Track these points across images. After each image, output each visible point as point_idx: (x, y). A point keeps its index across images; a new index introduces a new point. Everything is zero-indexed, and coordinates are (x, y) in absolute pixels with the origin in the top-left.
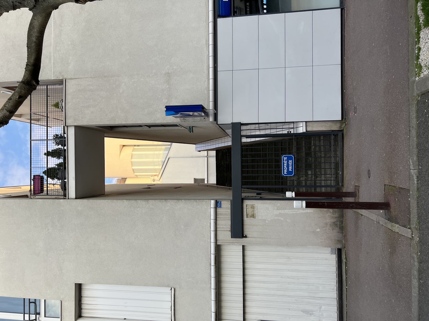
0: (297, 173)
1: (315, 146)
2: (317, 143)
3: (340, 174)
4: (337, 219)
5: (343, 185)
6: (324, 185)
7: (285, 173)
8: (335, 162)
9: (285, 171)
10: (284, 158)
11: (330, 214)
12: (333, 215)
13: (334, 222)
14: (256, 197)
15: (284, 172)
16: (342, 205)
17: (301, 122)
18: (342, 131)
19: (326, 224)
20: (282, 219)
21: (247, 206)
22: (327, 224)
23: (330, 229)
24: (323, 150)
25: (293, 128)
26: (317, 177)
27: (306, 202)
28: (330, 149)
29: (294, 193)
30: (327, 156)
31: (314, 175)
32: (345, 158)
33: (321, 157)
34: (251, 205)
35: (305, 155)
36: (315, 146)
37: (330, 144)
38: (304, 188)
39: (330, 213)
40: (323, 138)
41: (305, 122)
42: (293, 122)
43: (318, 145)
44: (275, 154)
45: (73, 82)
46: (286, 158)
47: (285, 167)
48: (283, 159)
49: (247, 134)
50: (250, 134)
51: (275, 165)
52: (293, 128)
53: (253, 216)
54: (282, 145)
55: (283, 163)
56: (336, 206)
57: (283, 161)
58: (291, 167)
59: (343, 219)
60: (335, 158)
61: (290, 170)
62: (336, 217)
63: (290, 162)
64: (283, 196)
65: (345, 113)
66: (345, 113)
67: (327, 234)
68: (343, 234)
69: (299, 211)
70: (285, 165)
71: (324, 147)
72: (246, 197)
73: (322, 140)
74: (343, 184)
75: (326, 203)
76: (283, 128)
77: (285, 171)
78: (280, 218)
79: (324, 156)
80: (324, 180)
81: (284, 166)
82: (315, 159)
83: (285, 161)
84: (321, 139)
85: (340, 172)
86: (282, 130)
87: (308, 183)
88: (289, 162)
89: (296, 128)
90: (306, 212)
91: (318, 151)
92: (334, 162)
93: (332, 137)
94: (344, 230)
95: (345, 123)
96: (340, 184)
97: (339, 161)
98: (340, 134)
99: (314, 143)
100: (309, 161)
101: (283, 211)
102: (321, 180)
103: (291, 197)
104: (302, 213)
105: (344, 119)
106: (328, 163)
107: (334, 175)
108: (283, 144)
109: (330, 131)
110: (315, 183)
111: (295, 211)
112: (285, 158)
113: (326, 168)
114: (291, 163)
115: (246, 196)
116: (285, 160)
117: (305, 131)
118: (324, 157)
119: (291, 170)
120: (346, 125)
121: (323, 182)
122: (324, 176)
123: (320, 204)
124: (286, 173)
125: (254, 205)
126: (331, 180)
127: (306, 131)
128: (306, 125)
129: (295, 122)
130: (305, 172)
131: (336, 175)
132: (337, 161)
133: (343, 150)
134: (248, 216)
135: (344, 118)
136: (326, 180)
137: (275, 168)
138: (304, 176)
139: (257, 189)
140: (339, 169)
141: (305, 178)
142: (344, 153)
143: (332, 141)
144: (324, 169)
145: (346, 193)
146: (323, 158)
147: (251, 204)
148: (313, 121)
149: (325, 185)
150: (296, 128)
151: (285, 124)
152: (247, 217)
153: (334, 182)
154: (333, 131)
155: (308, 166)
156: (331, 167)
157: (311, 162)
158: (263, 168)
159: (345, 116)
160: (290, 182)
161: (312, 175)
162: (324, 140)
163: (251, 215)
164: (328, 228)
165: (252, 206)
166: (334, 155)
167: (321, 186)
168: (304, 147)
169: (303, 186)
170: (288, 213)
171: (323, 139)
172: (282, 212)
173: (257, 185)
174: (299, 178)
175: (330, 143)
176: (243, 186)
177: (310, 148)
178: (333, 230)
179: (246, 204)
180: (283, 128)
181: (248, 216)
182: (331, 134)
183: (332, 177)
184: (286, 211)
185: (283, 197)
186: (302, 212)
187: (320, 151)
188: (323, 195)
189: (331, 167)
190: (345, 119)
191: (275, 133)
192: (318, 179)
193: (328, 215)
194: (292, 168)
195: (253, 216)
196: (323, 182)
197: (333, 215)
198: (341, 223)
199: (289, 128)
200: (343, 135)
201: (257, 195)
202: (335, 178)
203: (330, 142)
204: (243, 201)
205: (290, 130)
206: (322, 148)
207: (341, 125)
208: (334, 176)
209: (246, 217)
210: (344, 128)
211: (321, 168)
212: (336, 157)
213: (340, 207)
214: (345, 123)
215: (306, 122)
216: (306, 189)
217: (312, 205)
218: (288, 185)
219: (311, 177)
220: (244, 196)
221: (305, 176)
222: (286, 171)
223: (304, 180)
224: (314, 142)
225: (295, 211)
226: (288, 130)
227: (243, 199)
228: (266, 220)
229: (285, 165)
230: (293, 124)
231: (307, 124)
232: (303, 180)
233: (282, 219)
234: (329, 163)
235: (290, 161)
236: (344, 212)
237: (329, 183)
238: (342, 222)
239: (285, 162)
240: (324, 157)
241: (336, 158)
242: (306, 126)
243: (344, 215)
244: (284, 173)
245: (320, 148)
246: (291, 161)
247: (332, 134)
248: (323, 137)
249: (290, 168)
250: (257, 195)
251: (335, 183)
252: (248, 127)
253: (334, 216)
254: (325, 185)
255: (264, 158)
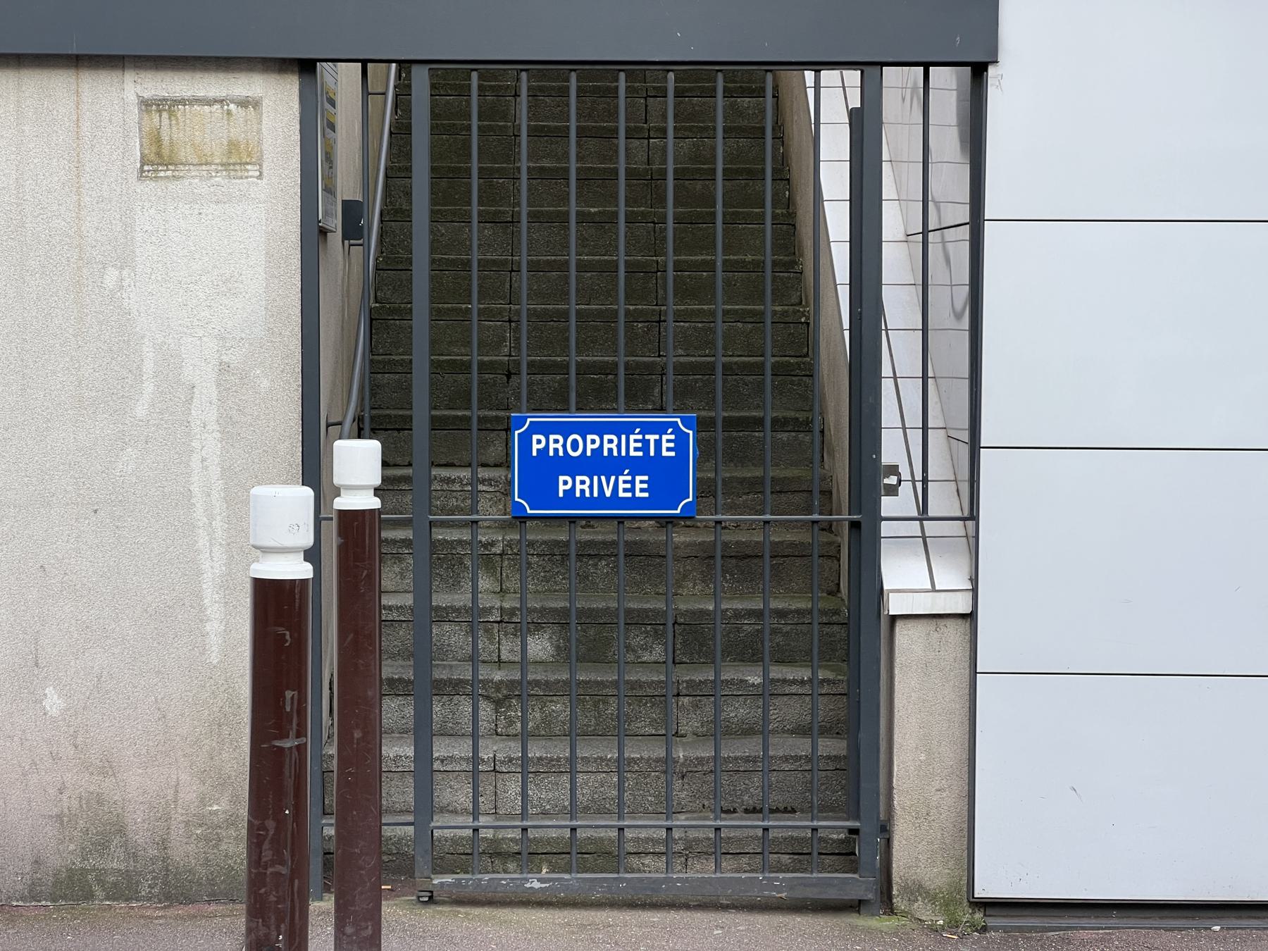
0: (531, 544)
1: (768, 692)
2: (788, 711)
3: (527, 880)
4: (153, 852)
5: (432, 900)
6: (436, 755)
7: (535, 437)
8: (630, 847)
9: (556, 444)
10: (665, 437)
11: (189, 794)
12: (187, 823)
13: (121, 831)
14: (330, 190)
15: (547, 429)
16: (284, 870)
17: (974, 580)
18: (886, 902)
19: (107, 768)
20: (141, 410)
21: (244, 103)
22: (103, 772)
23: (64, 797)
24: (724, 754)
25: (923, 515)
26: (498, 703)
27: (304, 582)
28: (735, 811)
29: (371, 502)
30: (678, 784)
31: (517, 676)
32: (655, 917)
33: (672, 736)
34: (260, 142)
35: (683, 614)
36: (768, 692)
37: (777, 811)
38: (408, 600)
39: (203, 801)
40: (829, 757)
41: (963, 606)
42: (973, 515)
43: (773, 714)
44: (709, 369)
45: (344, 196)
46: (665, 453)
47: (592, 443)
48: (660, 429)
49: (886, 168)
50: (885, 156)
51: (611, 369)
52: (923, 515)
53: (159, 154)
54: (779, 424)
55: (628, 429)
56: (271, 824)
57: (647, 428)
58: (586, 487)
59: (149, 899)
60: (655, 842)
61: (564, 483)
62: (164, 844)
63: (633, 482)
64: (340, 424)
65: (1031, 929)
66: (1031, 929)
67: (24, 775)
68: (22, 898)
69: (215, 549)
70: (610, 444)
71: (747, 760)
72: (327, 106)
73: (814, 747)
74: (443, 903)
75: (298, 747)
76: (925, 428)
77: (560, 438)
78: (149, 387)
79: (675, 761)
80: (475, 759)
81: (601, 429)
82: (650, 692)
83: (646, 443)
84: (821, 742)
85: (539, 880)
86: (914, 419)
87: (453, 637)
88: (633, 474)
89: (924, 538)
90: (202, 609)
91: (724, 715)
92: (629, 834)
93: (834, 827)
94: (58, 909)
95: (953, 925)
96: (448, 879)
97: (633, 871)
98: (858, 885)
99: (785, 681)
100: (634, 643)
101: (212, 415)
102: (475, 736)
103: (336, 481)
104: (199, 573)
105: (978, 915)
106: (615, 793)
107: (517, 834)
108: (784, 436)
109: (882, 808)
110: (453, 688)
111: (211, 518)
112: (665, 445)
113: (580, 778)
114: (621, 494)
115: (332, 103)
116: (652, 438)
117: (895, 606)
118: (668, 760)
119: (562, 488)
120: (934, 930)
121: (462, 749)
122: (511, 760)
123: (289, 694)
124: (535, 447)
125: (253, 171)
126: (475, 814)
127: (894, 619)
128: (942, 622)
129: (971, 532)
130: (542, 612)
131: (516, 848)
132: (634, 861)
133: (725, 908)
134: (160, 111)
135: (991, 922)
136: (475, 773)
137: (583, 369)
138: (507, 605)
139: (397, 213)
140: (567, 876)
141: (489, 611)
142: (699, 916)
143: (799, 825)
144: (572, 759)
145: (375, 917)
146: (663, 754)
147: (267, 146)
148: (974, 672)
149: (437, 766)
150: (924, 538)
151: (964, 451)
152: (146, 105)
153: (459, 832)
154: (885, 830)
155: (592, 632)
156: (586, 809)
157: (631, 657)
158: (579, 263)
159: (1006, 930)
160: (457, 487)
161: (524, 663)
162: (809, 759)
163: (166, 139)
164: (68, 777)
165: (249, 155)
166: (686, 840)
167: (423, 733)
168: (757, 604)
169: (423, 592)
170: (196, 458)
171: (822, 751)
172: (205, 411)
173: (435, 217)
174: (488, 561)
175: (785, 811)
176: (421, 79)
177: (748, 652)
178: (59, 817)
179: (265, 102)
180: (925, 428)
181: (160, 111)
182: (857, 818)
183: (498, 820)
184: (209, 446)
185: (328, 426)
186: (208, 576)
187: (718, 731)
188: (357, 734)
189: (586, 809)
190: (984, 929)
191: (886, 370)
192: (486, 710)
193: (184, 777)
194: (584, 502)
195: (159, 154)
196: (462, 749)
197: (187, 823)
198: (115, 885)
199: (925, 481)
200: (855, 907)
201: (346, 204)
202: (494, 841)
203: (793, 811)
204: (293, 72)
205: (905, 488)
206: (749, 747)
207: (931, 897)
208: (510, 834)
209: (147, 95)
210: (904, 914)
211: (573, 734)
212: (667, 850)
213: (267, 855)
214: (953, 925)
215: (970, 618)
216: (394, 615)
217: (281, 630)
218: (435, 472)
219: (499, 661)
220: (333, 86)
221: (512, 612)
222: (559, 446)
223: (474, 599)
224: (794, 682)
225: (211, 518)
226: (905, 473)
227: (306, 67)
228: (125, 273)
229: (610, 444)
230: (958, 514)
231: (950, 623)
232: (475, 592)
233: (141, 410)
234: (620, 797)
235: (638, 486)
236: (213, 907)
237: (455, 793)
238: (124, 889)
239: (632, 445)
240: (668, 760)
241: (663, 849)
242: (934, 621)
243: (191, 909)
244: (535, 428)
245: (747, 731)
246: (638, 494)
247: (856, 824)
248: (834, 753)
249: (583, 485)
250: (346, 204)
251: (455, 841)
252: (947, 142)
253: (178, 832)
254: (437, 766)
255: (671, 273)
